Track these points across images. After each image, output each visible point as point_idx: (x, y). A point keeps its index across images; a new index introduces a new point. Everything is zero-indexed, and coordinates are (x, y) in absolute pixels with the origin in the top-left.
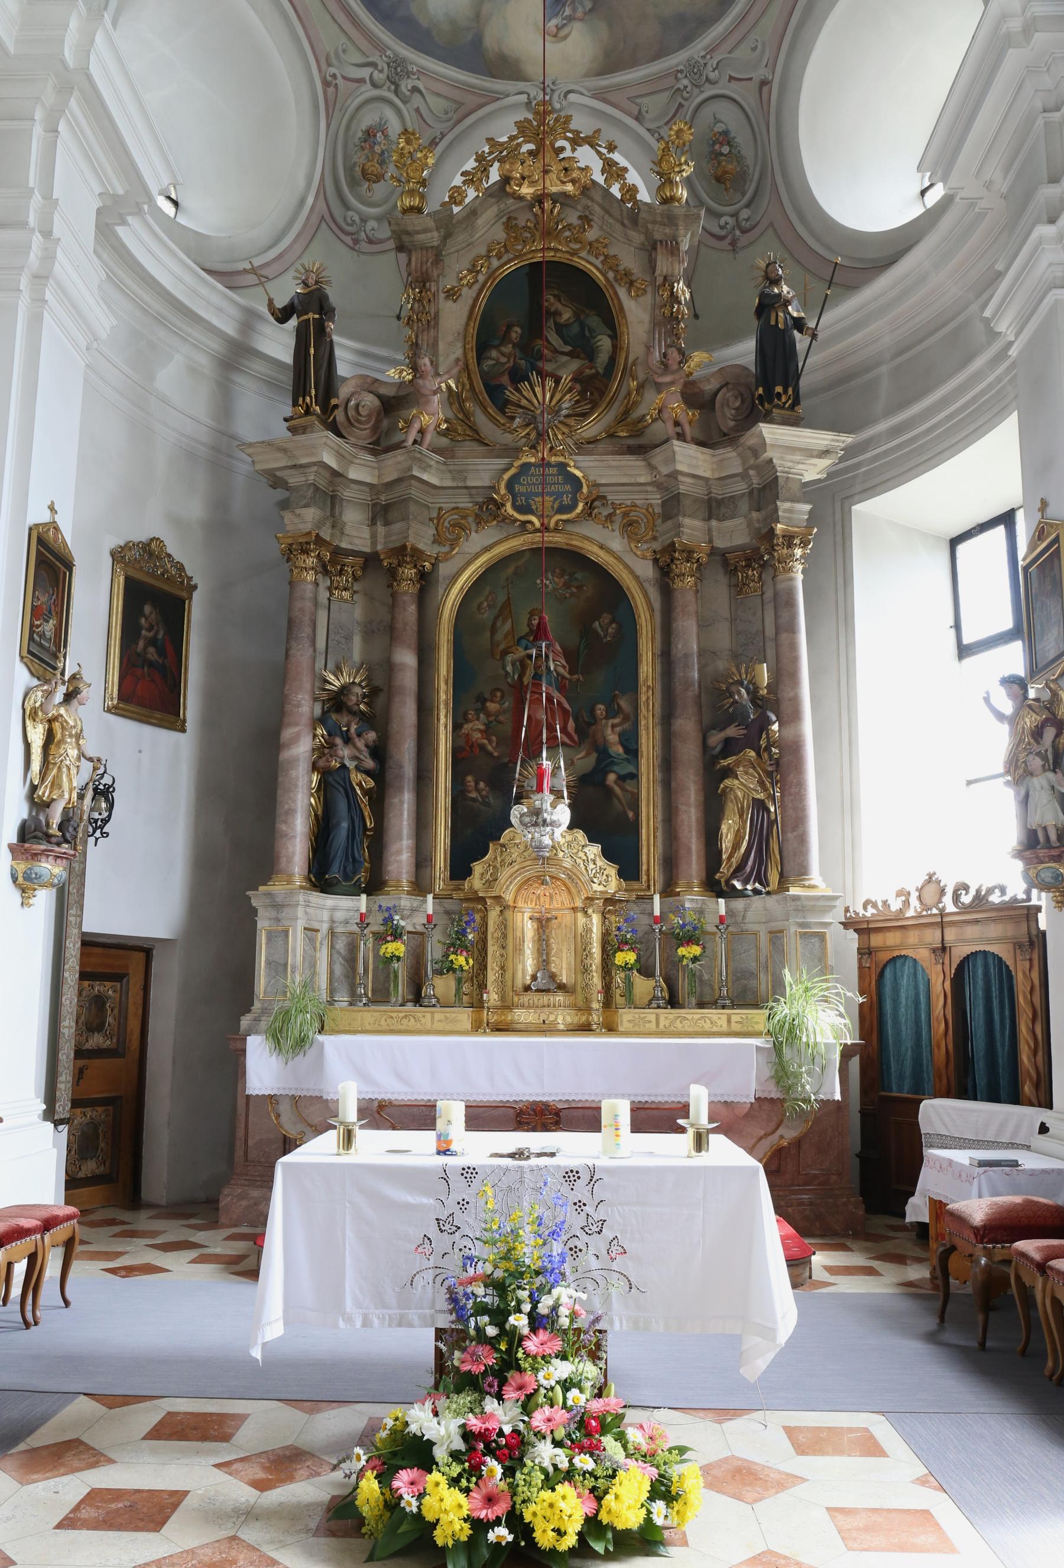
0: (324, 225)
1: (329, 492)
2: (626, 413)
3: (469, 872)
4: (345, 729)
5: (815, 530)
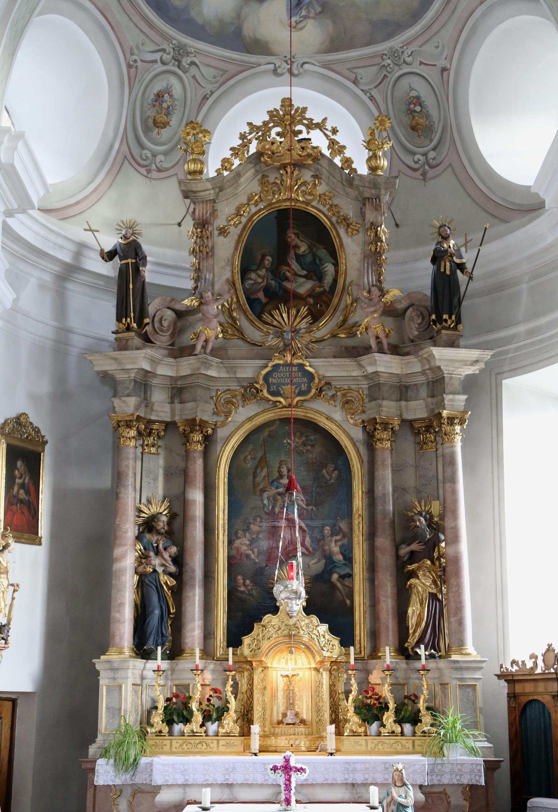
0: (126, 162)
1: (143, 384)
2: (345, 321)
4: (155, 545)
5: (470, 413)
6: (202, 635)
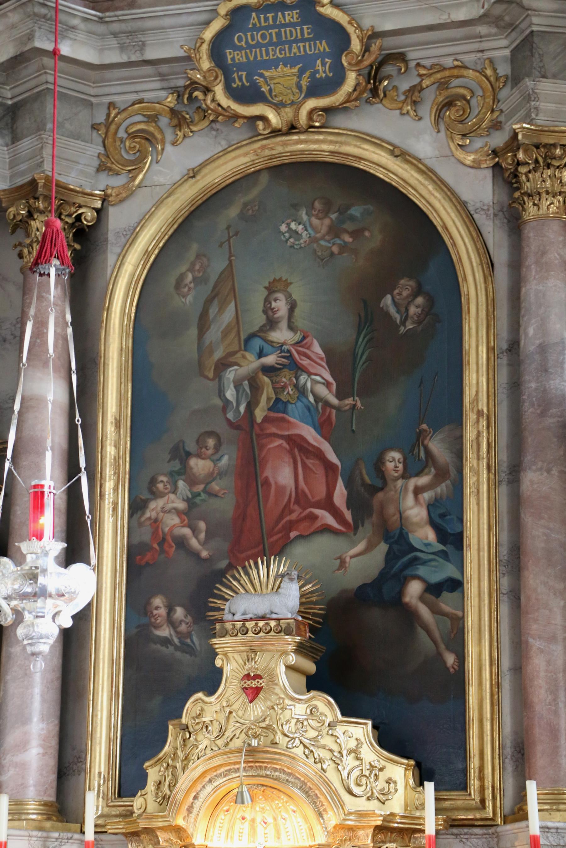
3: (141, 781)
6: (52, 762)
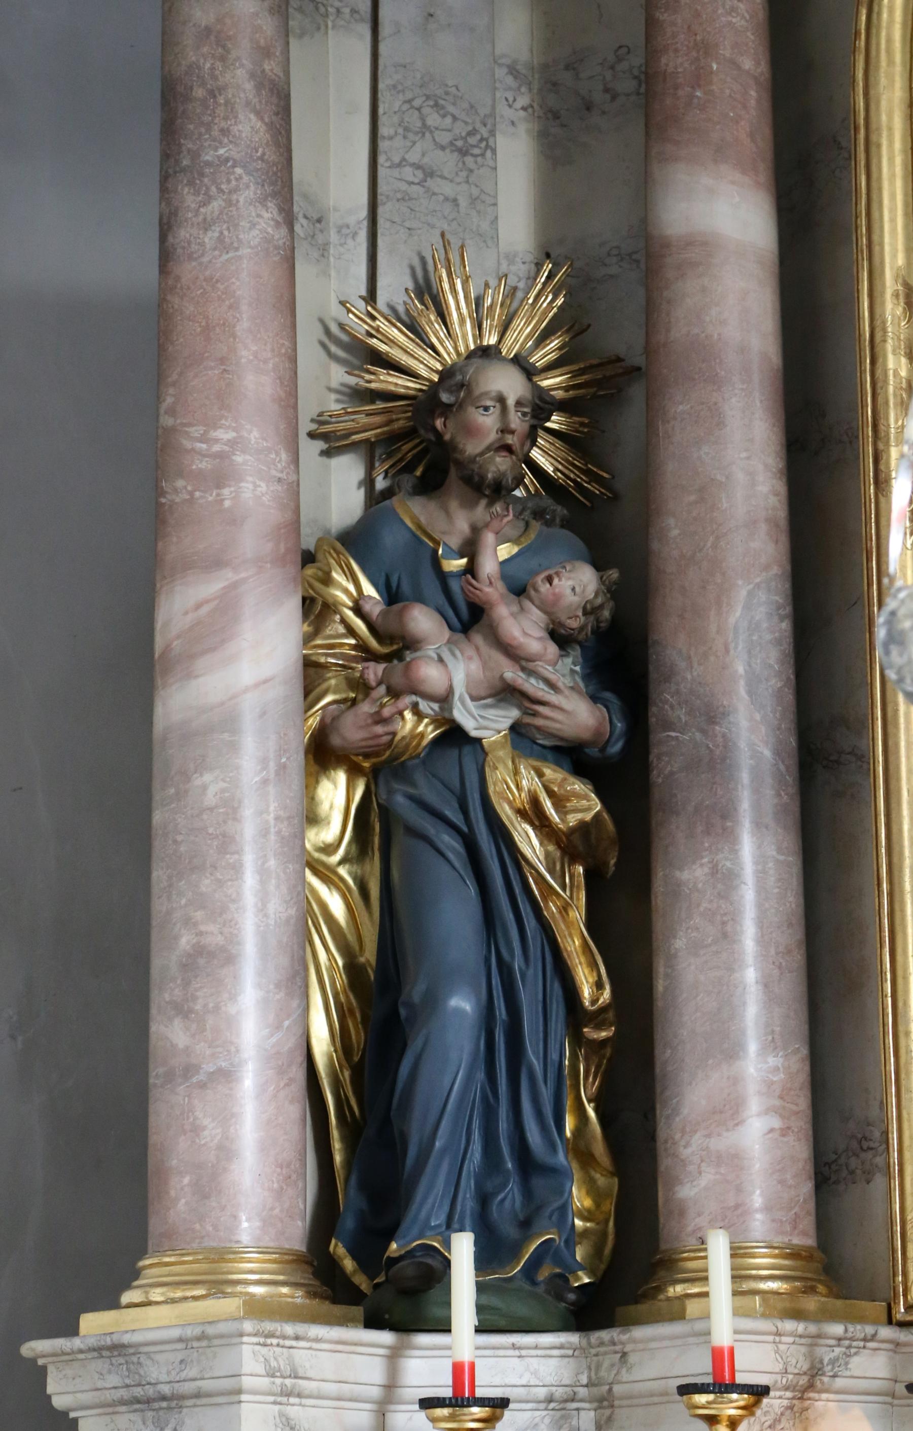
6: (800, 1150)
